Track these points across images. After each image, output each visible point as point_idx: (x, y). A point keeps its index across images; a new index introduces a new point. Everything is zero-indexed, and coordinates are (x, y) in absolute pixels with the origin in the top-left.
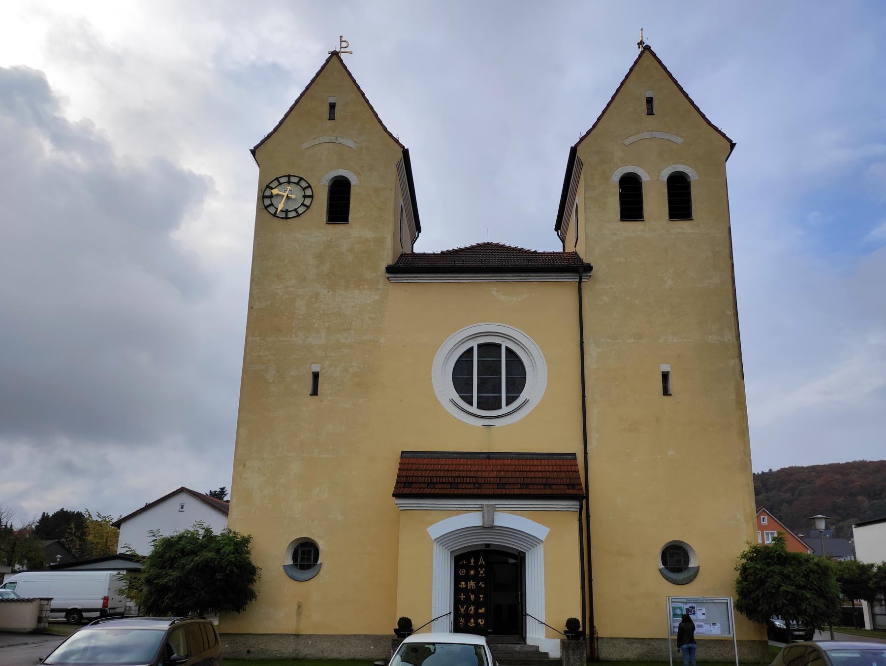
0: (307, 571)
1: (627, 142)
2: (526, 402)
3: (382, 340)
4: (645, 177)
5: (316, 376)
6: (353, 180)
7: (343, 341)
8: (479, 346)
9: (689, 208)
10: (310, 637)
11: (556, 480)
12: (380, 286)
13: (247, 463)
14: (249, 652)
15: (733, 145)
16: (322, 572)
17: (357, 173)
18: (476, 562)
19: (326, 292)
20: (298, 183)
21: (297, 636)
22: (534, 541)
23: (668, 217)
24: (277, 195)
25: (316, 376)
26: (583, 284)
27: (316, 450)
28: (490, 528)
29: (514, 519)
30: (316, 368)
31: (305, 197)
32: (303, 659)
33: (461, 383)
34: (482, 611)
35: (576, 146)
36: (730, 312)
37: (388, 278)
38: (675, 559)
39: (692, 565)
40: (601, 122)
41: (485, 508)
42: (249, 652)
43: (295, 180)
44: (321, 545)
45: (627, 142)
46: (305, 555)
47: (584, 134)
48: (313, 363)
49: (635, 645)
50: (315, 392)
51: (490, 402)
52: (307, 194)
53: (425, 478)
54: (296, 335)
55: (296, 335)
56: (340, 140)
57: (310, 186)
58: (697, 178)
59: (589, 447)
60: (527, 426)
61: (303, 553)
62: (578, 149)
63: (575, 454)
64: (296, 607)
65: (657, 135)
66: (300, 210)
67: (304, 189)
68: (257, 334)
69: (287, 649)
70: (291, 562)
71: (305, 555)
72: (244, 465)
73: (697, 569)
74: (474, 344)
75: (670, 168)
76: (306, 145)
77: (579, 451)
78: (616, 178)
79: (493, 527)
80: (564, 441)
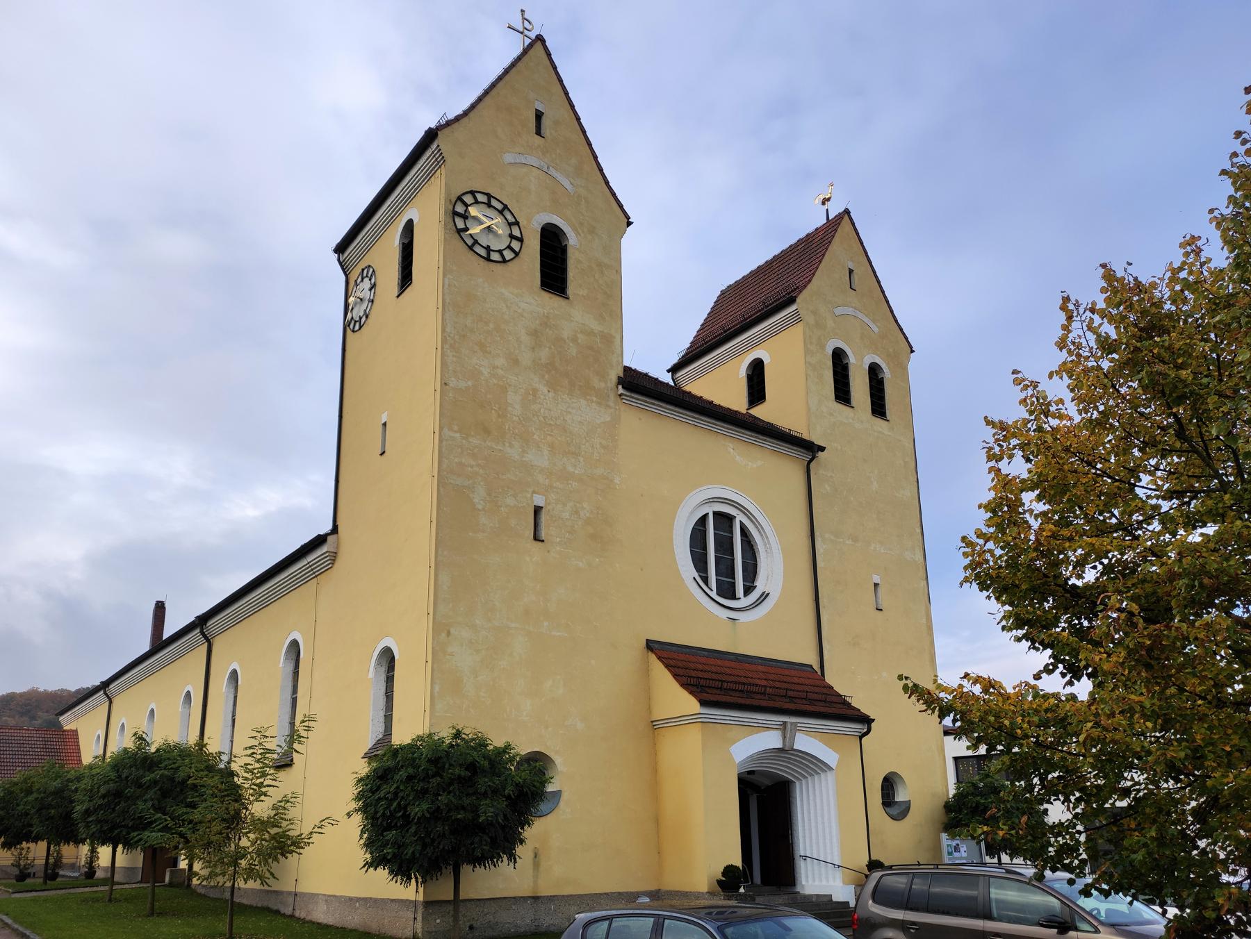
1: (838, 311)
2: (764, 596)
3: (617, 481)
7: (571, 469)
8: (715, 513)
10: (552, 899)
12: (611, 404)
13: (452, 631)
14: (471, 927)
15: (912, 351)
16: (562, 804)
17: (575, 230)
19: (545, 390)
20: (510, 225)
21: (536, 898)
24: (475, 218)
25: (537, 510)
27: (546, 624)
36: (919, 531)
42: (471, 927)
43: (516, 232)
44: (558, 760)
45: (838, 311)
48: (534, 492)
52: (505, 253)
54: (511, 446)
55: (511, 446)
56: (552, 172)
57: (517, 254)
60: (763, 628)
64: (532, 855)
65: (860, 315)
66: (508, 255)
68: (456, 428)
69: (523, 920)
72: (449, 633)
74: (710, 510)
76: (508, 158)
77: (816, 667)
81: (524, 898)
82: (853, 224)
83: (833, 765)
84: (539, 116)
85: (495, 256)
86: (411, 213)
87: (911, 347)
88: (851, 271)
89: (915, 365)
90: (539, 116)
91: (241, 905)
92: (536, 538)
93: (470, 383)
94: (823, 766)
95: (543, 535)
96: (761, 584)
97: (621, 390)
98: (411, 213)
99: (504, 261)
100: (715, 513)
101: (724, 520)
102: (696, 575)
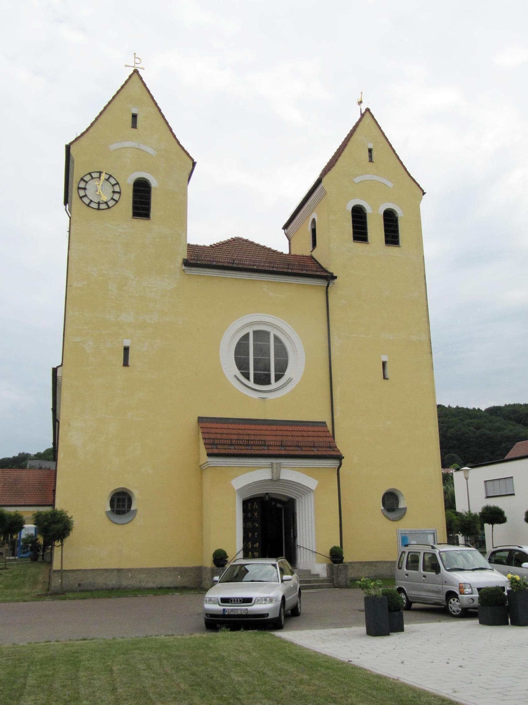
0: (123, 516)
2: (290, 380)
4: (369, 210)
5: (126, 350)
6: (154, 183)
8: (255, 332)
9: (366, 234)
10: (129, 570)
11: (314, 443)
15: (424, 193)
16: (137, 517)
18: (252, 506)
22: (306, 490)
23: (131, 214)
25: (126, 350)
26: (329, 288)
28: (276, 481)
29: (295, 474)
30: (127, 343)
31: (85, 189)
32: (125, 588)
33: (242, 365)
34: (257, 545)
35: (71, 143)
37: (184, 270)
38: (391, 501)
39: (401, 506)
40: (94, 127)
41: (275, 465)
42: (79, 585)
46: (121, 503)
47: (79, 135)
49: (366, 567)
50: (126, 363)
51: (262, 379)
52: (116, 190)
53: (226, 439)
58: (402, 215)
59: (335, 417)
60: (286, 401)
61: (119, 500)
62: (71, 146)
63: (325, 423)
66: (111, 203)
67: (113, 185)
70: (109, 509)
71: (121, 503)
72: (69, 425)
73: (405, 509)
74: (250, 330)
75: (395, 206)
78: (350, 209)
79: (279, 480)
80: (317, 413)
81: (113, 570)
82: (373, 117)
83: (313, 487)
84: (134, 116)
85: (103, 206)
86: (314, 215)
87: (423, 191)
88: (370, 151)
89: (426, 206)
90: (134, 116)
91: (65, 571)
92: (385, 378)
93: (85, 283)
94: (308, 490)
95: (387, 376)
96: (288, 374)
97: (184, 268)
98: (314, 215)
99: (109, 207)
100: (255, 332)
101: (261, 336)
102: (238, 373)
